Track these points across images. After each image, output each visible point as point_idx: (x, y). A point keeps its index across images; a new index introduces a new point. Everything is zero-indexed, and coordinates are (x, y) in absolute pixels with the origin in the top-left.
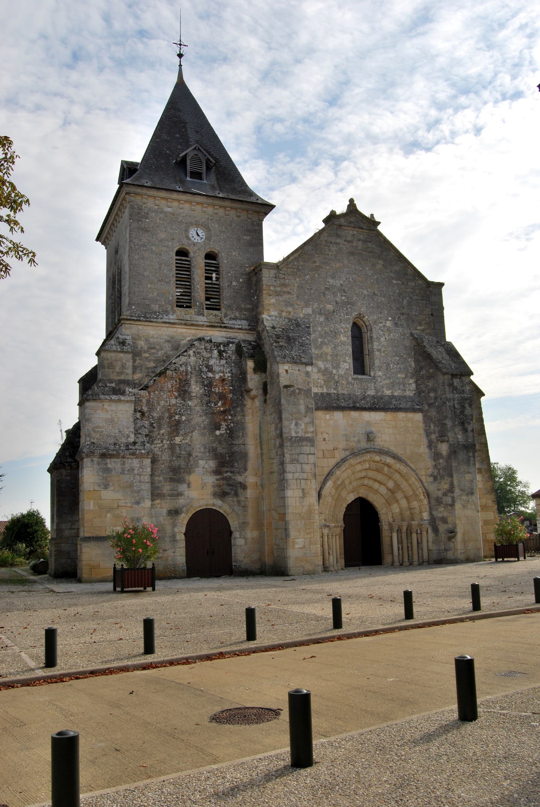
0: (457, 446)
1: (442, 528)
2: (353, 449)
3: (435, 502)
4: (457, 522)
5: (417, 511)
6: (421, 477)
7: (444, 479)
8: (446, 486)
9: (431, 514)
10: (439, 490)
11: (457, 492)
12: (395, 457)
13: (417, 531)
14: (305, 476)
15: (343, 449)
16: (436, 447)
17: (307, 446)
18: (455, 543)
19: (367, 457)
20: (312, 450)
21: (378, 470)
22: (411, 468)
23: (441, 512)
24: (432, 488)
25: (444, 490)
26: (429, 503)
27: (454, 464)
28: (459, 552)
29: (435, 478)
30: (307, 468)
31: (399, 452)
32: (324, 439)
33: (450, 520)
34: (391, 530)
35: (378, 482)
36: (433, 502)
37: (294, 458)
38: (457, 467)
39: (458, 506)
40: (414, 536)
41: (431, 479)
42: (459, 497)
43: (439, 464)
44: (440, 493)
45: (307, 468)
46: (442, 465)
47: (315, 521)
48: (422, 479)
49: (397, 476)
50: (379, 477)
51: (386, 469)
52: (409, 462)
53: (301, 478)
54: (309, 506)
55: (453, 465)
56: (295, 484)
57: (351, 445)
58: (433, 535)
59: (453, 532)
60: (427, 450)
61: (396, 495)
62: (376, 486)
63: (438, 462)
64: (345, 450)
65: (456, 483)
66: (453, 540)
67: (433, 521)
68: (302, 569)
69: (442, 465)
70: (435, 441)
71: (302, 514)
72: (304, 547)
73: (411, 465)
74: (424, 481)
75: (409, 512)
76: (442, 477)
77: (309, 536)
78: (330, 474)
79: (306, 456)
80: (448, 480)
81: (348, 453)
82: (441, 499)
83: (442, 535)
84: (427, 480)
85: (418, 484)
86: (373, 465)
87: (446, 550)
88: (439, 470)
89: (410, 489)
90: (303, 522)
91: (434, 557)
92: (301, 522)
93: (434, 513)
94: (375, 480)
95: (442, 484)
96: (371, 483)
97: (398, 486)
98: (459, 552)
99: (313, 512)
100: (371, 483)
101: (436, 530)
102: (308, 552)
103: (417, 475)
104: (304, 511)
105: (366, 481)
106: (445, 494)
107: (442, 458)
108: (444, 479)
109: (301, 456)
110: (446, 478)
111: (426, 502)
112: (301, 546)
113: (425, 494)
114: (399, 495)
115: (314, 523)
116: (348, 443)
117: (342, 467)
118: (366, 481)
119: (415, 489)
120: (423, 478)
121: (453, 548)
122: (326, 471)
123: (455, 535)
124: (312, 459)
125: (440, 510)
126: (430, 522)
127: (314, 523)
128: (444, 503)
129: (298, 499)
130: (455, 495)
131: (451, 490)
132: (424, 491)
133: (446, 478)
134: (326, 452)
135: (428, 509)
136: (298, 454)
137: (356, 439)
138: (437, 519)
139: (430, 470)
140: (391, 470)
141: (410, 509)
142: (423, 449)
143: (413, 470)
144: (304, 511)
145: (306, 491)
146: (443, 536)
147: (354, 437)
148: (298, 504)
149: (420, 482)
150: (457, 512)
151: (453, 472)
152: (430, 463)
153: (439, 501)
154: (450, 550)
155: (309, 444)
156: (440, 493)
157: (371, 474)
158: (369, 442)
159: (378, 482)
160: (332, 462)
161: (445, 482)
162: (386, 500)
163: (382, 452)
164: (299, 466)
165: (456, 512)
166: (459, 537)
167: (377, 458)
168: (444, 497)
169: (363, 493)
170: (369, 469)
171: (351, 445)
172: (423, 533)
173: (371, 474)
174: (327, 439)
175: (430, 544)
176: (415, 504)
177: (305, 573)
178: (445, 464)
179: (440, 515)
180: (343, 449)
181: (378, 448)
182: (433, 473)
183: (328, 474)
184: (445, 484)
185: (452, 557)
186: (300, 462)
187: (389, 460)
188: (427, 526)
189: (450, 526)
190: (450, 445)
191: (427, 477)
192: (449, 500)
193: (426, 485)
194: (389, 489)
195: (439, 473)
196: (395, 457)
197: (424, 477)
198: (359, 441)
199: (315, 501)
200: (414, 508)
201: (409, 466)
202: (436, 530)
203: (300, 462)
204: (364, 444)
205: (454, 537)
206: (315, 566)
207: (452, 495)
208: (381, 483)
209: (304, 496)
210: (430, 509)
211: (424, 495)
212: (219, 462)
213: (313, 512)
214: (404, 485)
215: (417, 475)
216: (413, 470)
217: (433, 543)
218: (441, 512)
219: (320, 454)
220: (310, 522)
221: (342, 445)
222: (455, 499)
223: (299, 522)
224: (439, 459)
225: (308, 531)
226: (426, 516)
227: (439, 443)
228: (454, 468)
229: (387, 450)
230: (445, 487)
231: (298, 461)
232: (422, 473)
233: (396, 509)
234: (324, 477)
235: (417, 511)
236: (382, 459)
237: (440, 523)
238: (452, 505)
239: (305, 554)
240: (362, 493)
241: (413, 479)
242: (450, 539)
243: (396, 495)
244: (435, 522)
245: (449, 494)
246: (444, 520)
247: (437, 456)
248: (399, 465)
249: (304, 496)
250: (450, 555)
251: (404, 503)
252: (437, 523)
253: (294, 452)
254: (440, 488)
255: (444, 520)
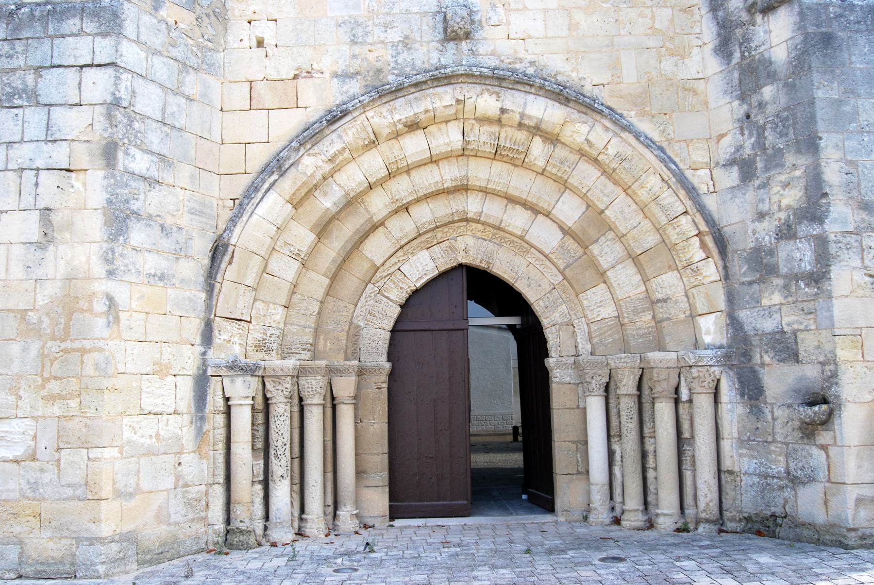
0: (838, 16)
1: (778, 379)
2: (379, 71)
3: (748, 268)
4: (842, 354)
5: (678, 311)
6: (688, 173)
7: (782, 165)
8: (793, 197)
9: (734, 323)
10: (761, 216)
11: (841, 214)
12: (562, 94)
13: (677, 390)
14: (60, 155)
15: (335, 75)
16: (746, 40)
17: (81, 33)
18: (832, 451)
19: (443, 98)
20: (104, 49)
21: (516, 159)
22: (637, 136)
23: (770, 311)
24: (734, 213)
25: (783, 215)
26: (727, 276)
27: (825, 92)
28: (852, 494)
29: (746, 169)
30: (71, 122)
31: (588, 76)
32: (260, 44)
33: (807, 343)
34: (581, 383)
35: (525, 205)
36: (740, 270)
37: (18, 84)
38: (840, 102)
39: (845, 277)
40: (664, 411)
41: (732, 177)
42: (852, 239)
43: (761, 105)
44: (765, 231)
45: (71, 122)
46: (770, 109)
47: (87, 344)
48: (696, 182)
49: (586, 175)
50: (520, 183)
51: (538, 149)
52: (632, 117)
53: (39, 163)
54: (69, 279)
55: (820, 94)
56: (14, 188)
57: (371, 57)
58: (740, 410)
59: (825, 401)
60: (714, 65)
61: (595, 249)
62: (517, 219)
63: (755, 99)
64: (345, 76)
65: (832, 174)
66: (824, 437)
67: (739, 354)
68: (12, 554)
69: (770, 109)
70: (745, 16)
71: (33, 316)
72: (33, 458)
73: (644, 126)
74: (703, 189)
75: (647, 317)
76: (774, 160)
77: (56, 410)
78: (277, 166)
79: (71, 75)
80: (797, 164)
81: (355, 87)
82: (771, 252)
83: (778, 413)
84: (718, 187)
85: (675, 201)
86: (482, 136)
87: (794, 481)
88: (761, 136)
89: (646, 225)
90: (35, 348)
91: (746, 500)
92: (25, 350)
93: (743, 315)
94: (511, 200)
95: (776, 189)
96: (493, 210)
97: (596, 216)
98: (852, 494)
99: (83, 304)
100: (493, 210)
101: (752, 390)
102: (46, 478)
103: (667, 161)
104: (40, 303)
105: (473, 204)
106: (786, 233)
107: (772, 77)
108: (782, 165)
109: (50, 76)
110: (790, 159)
111: (711, 271)
112: (18, 451)
113: (709, 241)
114: (606, 252)
115: (84, 351)
116: (357, 50)
117: (326, 142)
118: (473, 204)
119: (664, 220)
120: (700, 179)
121: (822, 475)
122: (259, 156)
123: (831, 414)
124: (98, 85)
125: (765, 302)
126: (727, 357)
127: (84, 351)
128: (784, 270)
129: (17, 251)
130: (831, 228)
131: (813, 209)
132: (704, 227)
133: (790, 159)
134: (261, 88)
135: (721, 303)
136: (38, 69)
137: (394, 36)
138: (755, 341)
139: (726, 141)
140: (560, 152)
141: (653, 303)
142: (703, 64)
143: (649, 143)
144: (40, 303)
145: (56, 218)
146: (782, 417)
147: (386, 26)
148: (17, 271)
149: (682, 193)
150: (839, 309)
151: (821, 126)
152: (725, 111)
153: (762, 264)
154: (812, 480)
155: (90, 27)
156: (765, 231)
157: (481, 172)
158: (451, 45)
159: (525, 205)
160: (288, 124)
161: (783, 178)
162: (562, 273)
163: (501, 79)
164: (35, 117)
165: (838, 307)
166: (851, 423)
167: (487, 103)
168: (782, 243)
169: (471, 250)
170: (464, 153)
171: (371, 57)
172: (697, 399)
173: (481, 172)
174: (269, 41)
175: (727, 445)
176: (669, 283)
177: (28, 570)
178: (783, 101)
179: (768, 325)
180: (335, 75)
181: (493, 62)
182: (739, 148)
183: (266, 170)
184: (786, 185)
185: (820, 517)
186: (43, 100)
187: (541, 109)
188: (717, 370)
189: (811, 372)
190: (802, 14)
191: (717, 172)
192: (800, 254)
193: (711, 203)
194: (566, 231)
195: (760, 144)
196: (562, 94)
197: (704, 173)
198: (406, 43)
199: (94, 259)
200: (665, 301)
201: (627, 128)
202: (752, 390)
203: (43, 100)
204: (428, 54)
205: (826, 422)
206: (79, 540)
207: (816, 230)
208: (535, 210)
209: (48, 236)
210: (731, 298)
211: (703, 246)
212: (780, 291)
213: (83, 304)
214: (620, 210)
215: (667, 161)
216: (649, 143)
217: (742, 442)
218: (770, 311)
219: (239, 96)
220: (66, 351)
221: (334, 56)
222: (833, 249)
223: (15, 349)
224: (758, 88)
225: (54, 387)
226: (712, 330)
227: (759, 18)
228: (821, 112)
229: (531, 71)
230: (785, 202)
231: (33, 97)
232: (697, 162)
233: (598, 305)
234: (245, 181)
235: (678, 311)
236: (508, 105)
237: (767, 359)
238: (818, 277)
239: (34, 486)
240: (465, 251)
241: (653, 182)
242: (809, 430)
243: (595, 249)
244: (747, 355)
245: (803, 229)
246: (786, 348)
247: (751, 75)
248: (584, 129)
249: (48, 236)
250: (808, 504)
251: (626, 281)
252: (757, 359)
253: (20, 62)
254: (765, 207)
255: (786, 348)
